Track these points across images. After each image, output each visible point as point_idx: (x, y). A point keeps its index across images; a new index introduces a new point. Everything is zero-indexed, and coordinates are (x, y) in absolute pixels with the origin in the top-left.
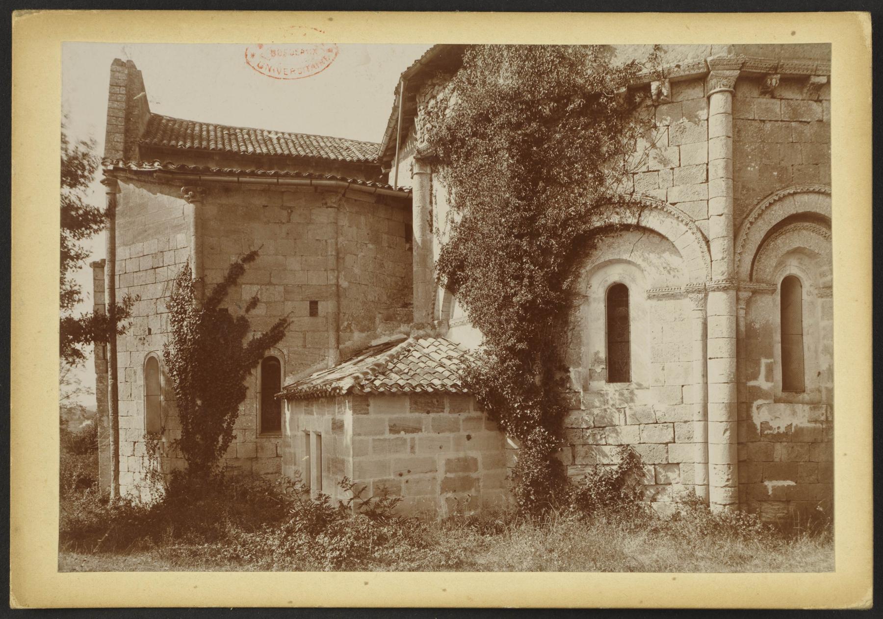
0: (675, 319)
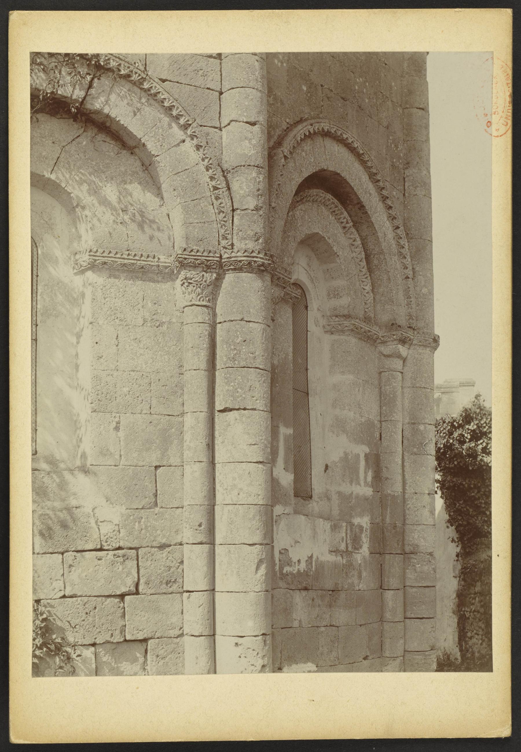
0: (145, 321)
